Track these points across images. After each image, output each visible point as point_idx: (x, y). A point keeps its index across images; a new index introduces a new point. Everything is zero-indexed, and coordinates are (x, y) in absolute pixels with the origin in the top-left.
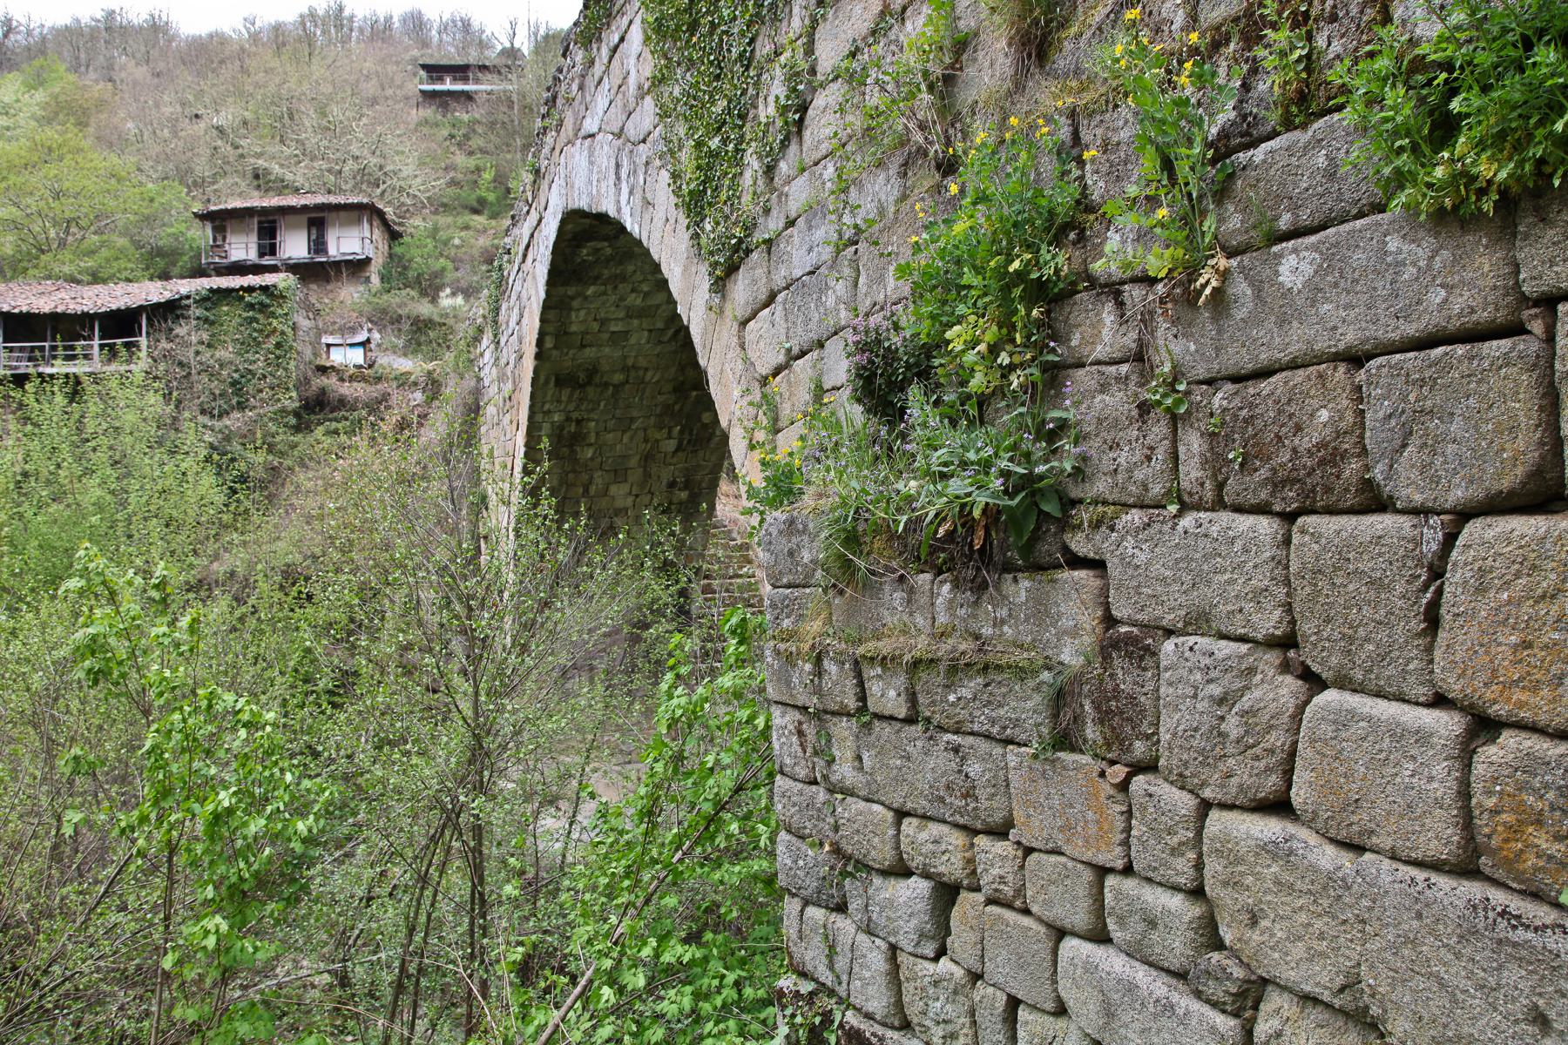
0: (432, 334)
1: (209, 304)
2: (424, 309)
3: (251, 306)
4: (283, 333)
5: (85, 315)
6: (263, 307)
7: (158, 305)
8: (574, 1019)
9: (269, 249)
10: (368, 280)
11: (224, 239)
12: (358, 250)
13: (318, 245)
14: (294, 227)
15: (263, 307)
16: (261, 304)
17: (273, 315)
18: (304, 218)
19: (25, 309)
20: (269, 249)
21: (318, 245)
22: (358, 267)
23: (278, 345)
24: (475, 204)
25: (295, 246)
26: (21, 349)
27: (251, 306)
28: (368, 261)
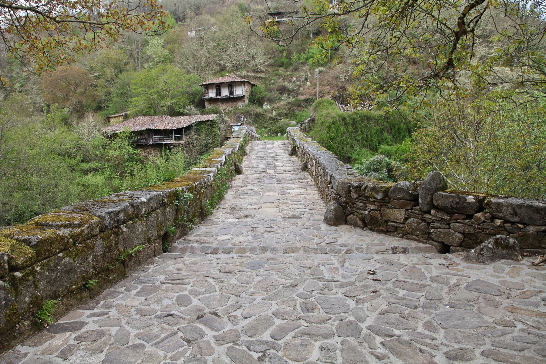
0: (260, 118)
1: (198, 125)
2: (259, 110)
3: (208, 125)
4: (216, 131)
5: (171, 130)
6: (211, 125)
7: (187, 127)
8: (398, 22)
9: (219, 94)
10: (244, 101)
11: (208, 91)
12: (241, 94)
13: (231, 93)
14: (225, 87)
15: (211, 125)
16: (210, 124)
17: (214, 127)
18: (227, 84)
19: (158, 128)
20: (219, 94)
21: (231, 93)
22: (240, 98)
23: (215, 135)
24: (281, 64)
25: (225, 93)
26: (158, 138)
27: (208, 125)
28: (244, 96)
